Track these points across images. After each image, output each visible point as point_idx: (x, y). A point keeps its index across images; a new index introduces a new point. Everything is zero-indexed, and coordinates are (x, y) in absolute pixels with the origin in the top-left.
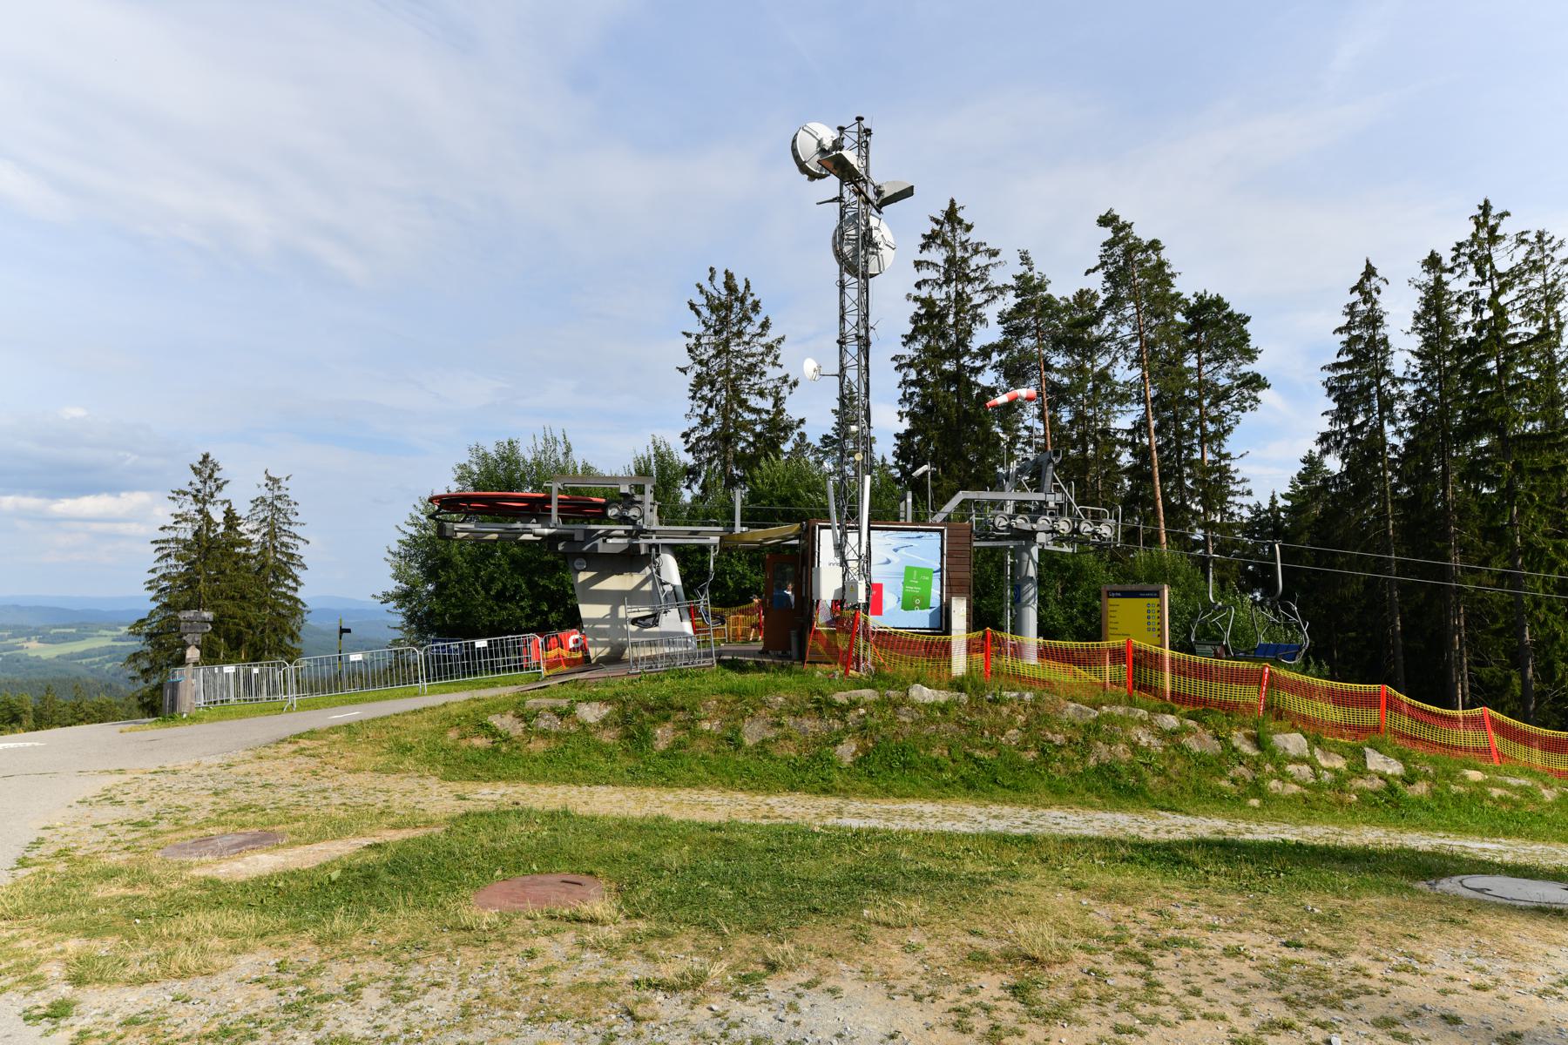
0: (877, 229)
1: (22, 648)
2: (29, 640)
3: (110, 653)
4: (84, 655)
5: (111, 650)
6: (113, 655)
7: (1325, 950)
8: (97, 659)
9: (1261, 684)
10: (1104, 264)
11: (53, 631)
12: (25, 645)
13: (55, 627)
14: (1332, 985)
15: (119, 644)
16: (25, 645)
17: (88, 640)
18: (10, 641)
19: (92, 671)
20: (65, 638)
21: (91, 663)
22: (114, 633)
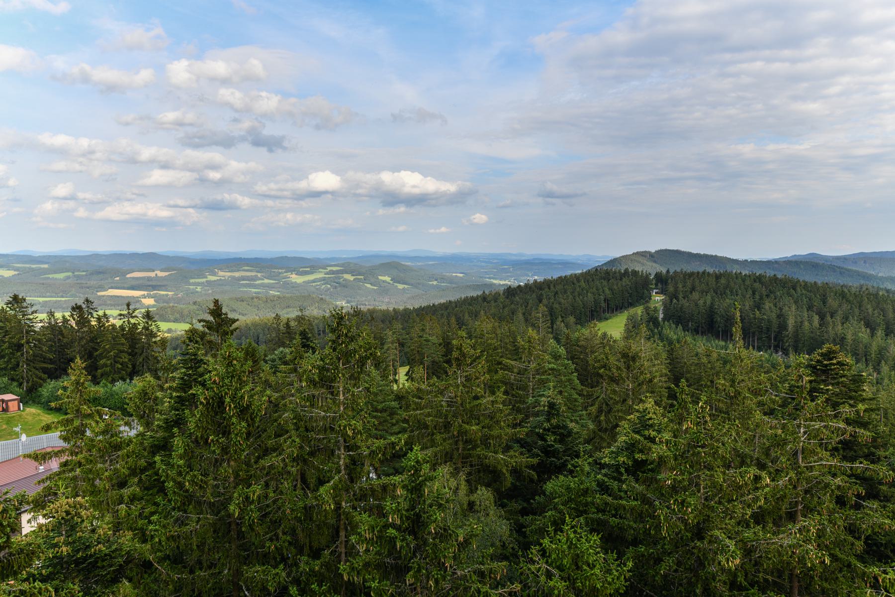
0: (51, 314)
1: (289, 277)
2: (292, 274)
3: (324, 280)
4: (314, 281)
5: (324, 279)
6: (325, 282)
7: (119, 344)
8: (319, 283)
9: (790, 508)
10: (20, 514)
11: (301, 270)
12: (291, 276)
13: (302, 268)
14: (238, 371)
15: (327, 276)
16: (291, 276)
17: (315, 274)
18: (285, 274)
19: (317, 289)
20: (306, 273)
21: (317, 285)
22: (325, 271)
